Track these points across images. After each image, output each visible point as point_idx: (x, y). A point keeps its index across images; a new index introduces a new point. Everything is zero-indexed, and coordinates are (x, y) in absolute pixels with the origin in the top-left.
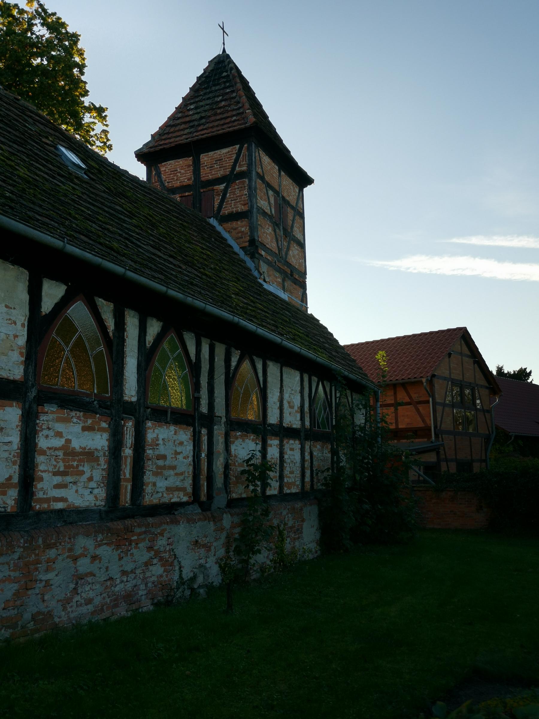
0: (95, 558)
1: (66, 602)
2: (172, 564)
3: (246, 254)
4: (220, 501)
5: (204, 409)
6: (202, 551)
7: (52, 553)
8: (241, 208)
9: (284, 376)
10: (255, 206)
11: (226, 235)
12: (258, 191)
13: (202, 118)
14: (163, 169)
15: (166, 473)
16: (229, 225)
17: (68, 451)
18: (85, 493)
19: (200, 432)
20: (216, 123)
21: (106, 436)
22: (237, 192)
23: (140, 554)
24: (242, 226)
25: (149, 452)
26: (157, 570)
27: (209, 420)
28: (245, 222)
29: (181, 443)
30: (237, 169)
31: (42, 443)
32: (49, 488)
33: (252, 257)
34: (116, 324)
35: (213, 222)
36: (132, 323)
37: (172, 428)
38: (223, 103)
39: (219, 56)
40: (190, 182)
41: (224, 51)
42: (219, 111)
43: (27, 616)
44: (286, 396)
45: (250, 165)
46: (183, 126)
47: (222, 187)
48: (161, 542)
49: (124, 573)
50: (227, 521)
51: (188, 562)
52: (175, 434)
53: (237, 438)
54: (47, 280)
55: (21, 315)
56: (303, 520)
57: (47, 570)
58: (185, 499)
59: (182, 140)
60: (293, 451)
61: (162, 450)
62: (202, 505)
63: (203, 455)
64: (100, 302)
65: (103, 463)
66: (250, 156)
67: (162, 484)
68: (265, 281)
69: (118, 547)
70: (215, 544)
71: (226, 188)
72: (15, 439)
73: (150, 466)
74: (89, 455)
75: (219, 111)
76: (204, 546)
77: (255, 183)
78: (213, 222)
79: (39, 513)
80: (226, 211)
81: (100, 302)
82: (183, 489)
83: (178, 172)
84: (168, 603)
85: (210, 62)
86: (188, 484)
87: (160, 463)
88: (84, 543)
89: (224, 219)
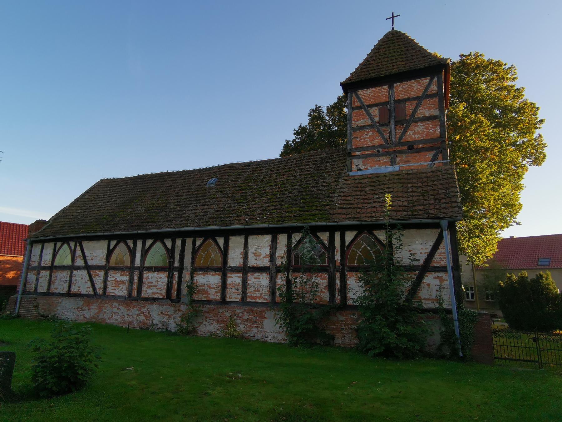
0: (118, 309)
1: (109, 318)
2: (149, 317)
4: (185, 299)
5: (177, 264)
6: (166, 317)
7: (106, 305)
15: (152, 288)
17: (116, 281)
18: (122, 292)
19: (173, 274)
21: (128, 277)
23: (135, 311)
25: (144, 281)
26: (142, 318)
27: (181, 269)
29: (161, 278)
31: (109, 279)
32: (110, 289)
34: (133, 246)
37: (156, 273)
41: (393, 29)
43: (100, 318)
48: (144, 309)
49: (128, 315)
50: (183, 308)
51: (157, 319)
52: (158, 274)
53: (199, 275)
54: (254, 237)
55: (106, 251)
56: (265, 318)
57: (105, 309)
58: (161, 297)
60: (264, 280)
61: (150, 280)
62: (172, 300)
63: (174, 282)
64: (128, 241)
65: (127, 284)
67: (149, 291)
69: (126, 307)
70: (174, 315)
72: (102, 278)
73: (144, 285)
74: (123, 282)
76: (166, 315)
79: (108, 295)
81: (128, 241)
82: (161, 294)
84: (147, 329)
86: (164, 292)
87: (149, 284)
88: (115, 304)
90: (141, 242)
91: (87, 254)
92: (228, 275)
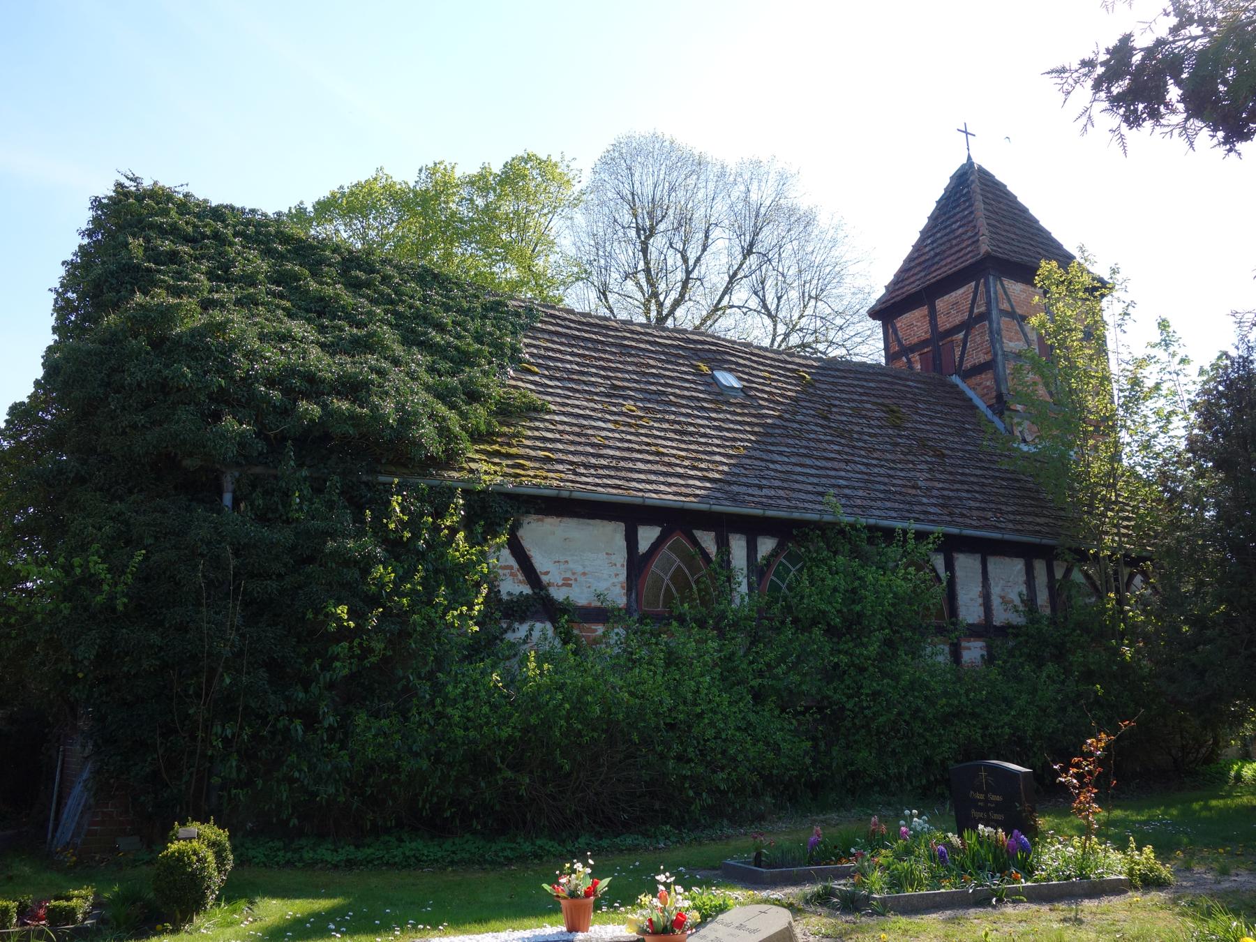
3: (994, 413)
8: (983, 358)
9: (990, 567)
10: (1000, 352)
11: (970, 393)
12: (1004, 333)
13: (936, 255)
14: (898, 325)
16: (976, 380)
20: (949, 260)
22: (978, 338)
24: (987, 380)
28: (990, 374)
30: (976, 311)
33: (1000, 414)
35: (955, 379)
36: (738, 546)
38: (960, 231)
39: (963, 166)
40: (928, 336)
41: (969, 158)
42: (954, 242)
44: (996, 591)
45: (988, 303)
46: (919, 269)
47: (961, 335)
55: (621, 557)
59: (912, 289)
64: (698, 534)
66: (988, 292)
68: (1024, 441)
71: (966, 336)
75: (954, 242)
77: (998, 323)
78: (955, 379)
80: (967, 364)
81: (698, 534)
83: (914, 324)
85: (952, 178)
89: (967, 375)
90: (743, 543)
91: (540, 562)
92: (964, 644)
